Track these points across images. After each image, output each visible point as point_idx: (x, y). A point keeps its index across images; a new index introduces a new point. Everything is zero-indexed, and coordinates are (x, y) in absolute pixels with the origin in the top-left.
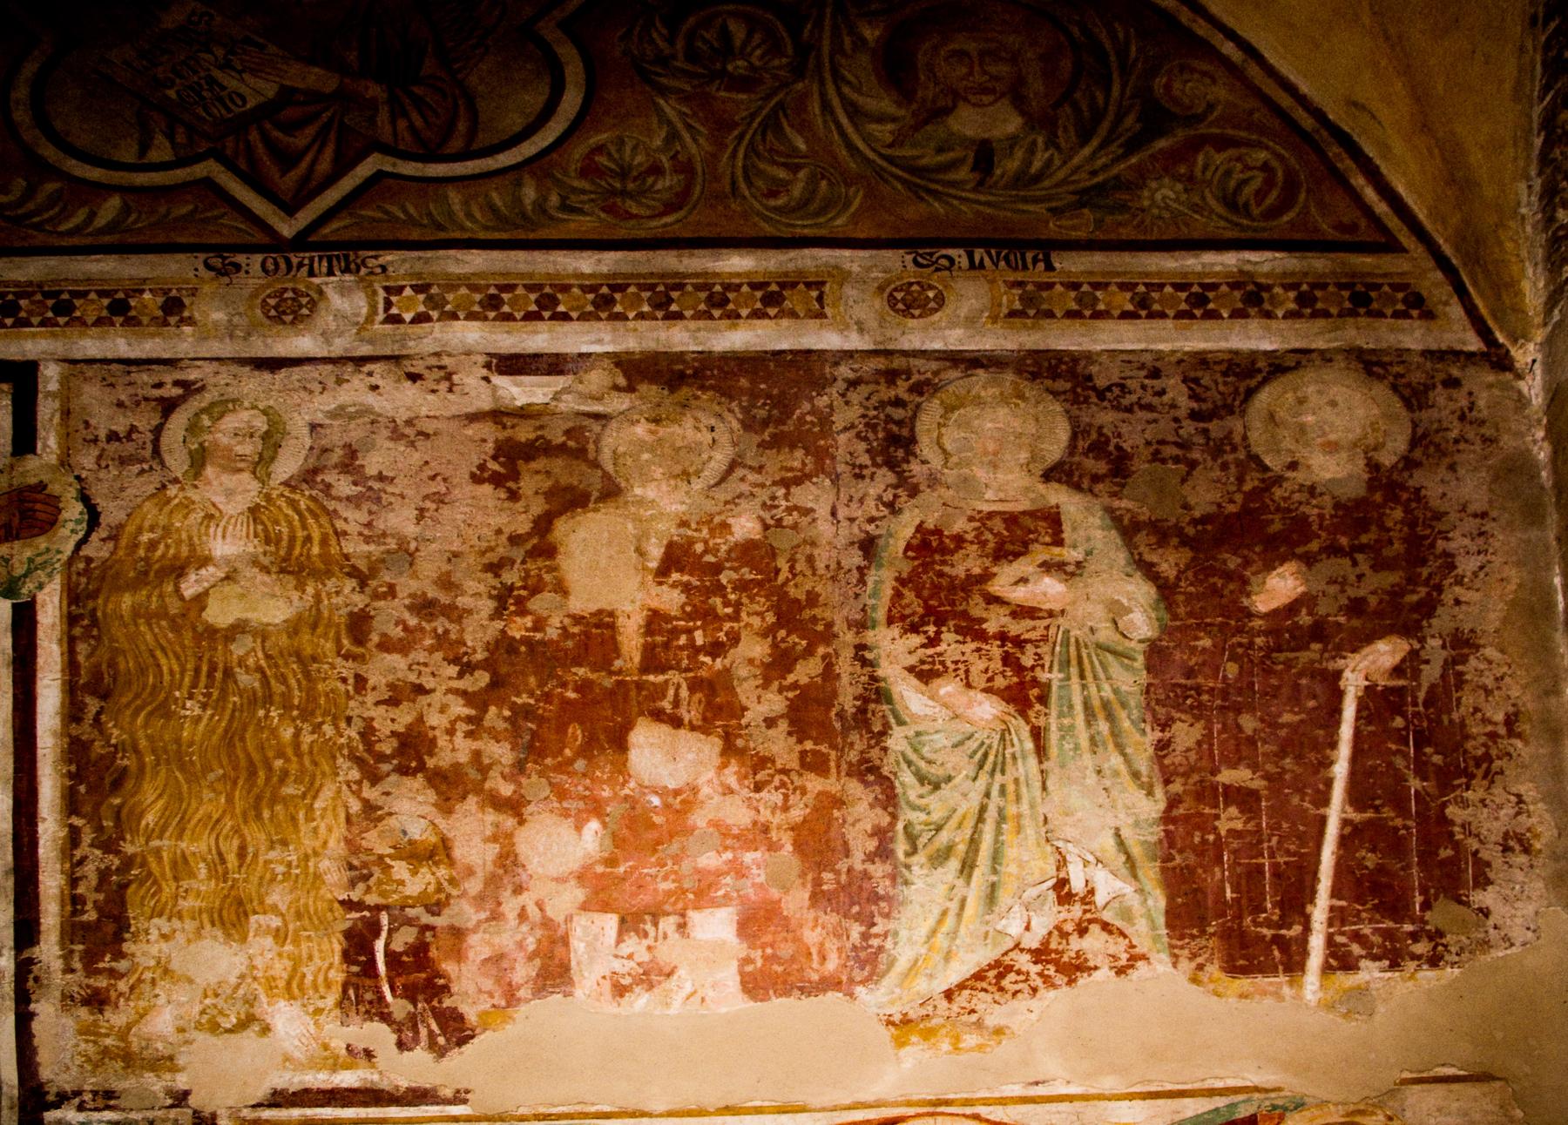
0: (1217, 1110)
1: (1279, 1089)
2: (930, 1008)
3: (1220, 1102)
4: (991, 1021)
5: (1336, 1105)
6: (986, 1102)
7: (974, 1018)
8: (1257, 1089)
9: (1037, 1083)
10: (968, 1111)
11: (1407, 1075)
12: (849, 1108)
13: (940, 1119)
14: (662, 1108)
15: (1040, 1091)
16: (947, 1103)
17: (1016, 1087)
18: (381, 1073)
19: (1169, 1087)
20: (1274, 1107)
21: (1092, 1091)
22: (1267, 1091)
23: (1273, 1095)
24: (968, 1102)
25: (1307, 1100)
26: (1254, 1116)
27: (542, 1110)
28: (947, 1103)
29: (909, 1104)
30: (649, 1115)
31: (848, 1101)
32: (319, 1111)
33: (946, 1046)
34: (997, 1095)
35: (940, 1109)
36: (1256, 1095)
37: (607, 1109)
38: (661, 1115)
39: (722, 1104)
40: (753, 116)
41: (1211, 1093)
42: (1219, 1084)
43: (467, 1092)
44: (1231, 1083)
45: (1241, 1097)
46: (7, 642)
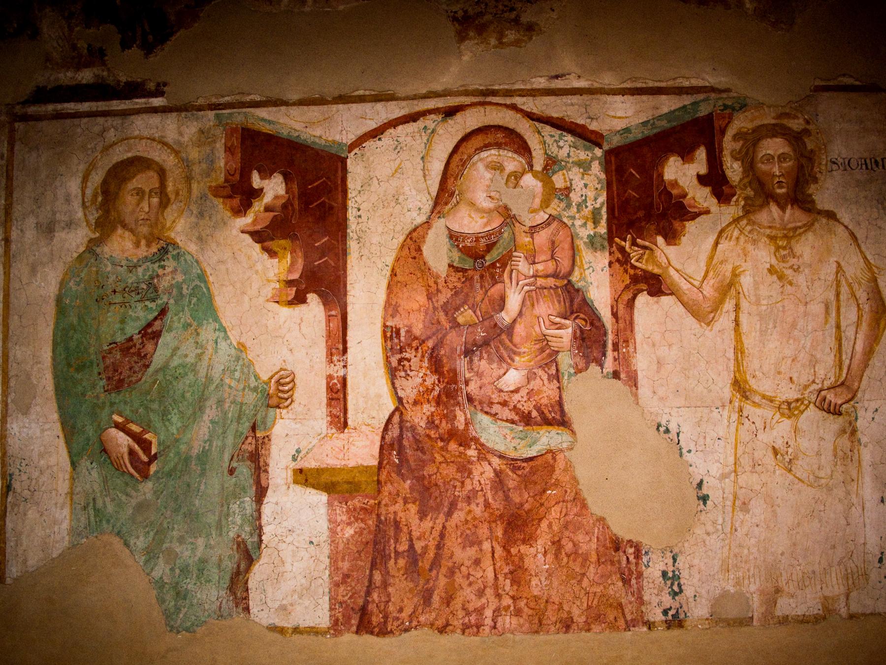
0: (684, 107)
1: (728, 90)
2: (483, 6)
3: (687, 100)
4: (525, 19)
5: (769, 107)
6: (523, 93)
7: (513, 15)
8: (712, 89)
9: (557, 77)
10: (508, 101)
11: (818, 83)
12: (426, 97)
13: (488, 108)
14: (295, 97)
15: (559, 84)
16: (494, 93)
17: (542, 80)
18: (109, 70)
19: (651, 84)
20: (726, 107)
21: (596, 85)
22: (720, 91)
23: (724, 95)
24: (509, 93)
25: (748, 101)
26: (711, 114)
27: (214, 100)
28: (494, 93)
29: (467, 93)
30: (286, 103)
31: (424, 91)
32: (66, 105)
33: (493, 41)
34: (528, 87)
35: (489, 99)
36: (713, 95)
37: (258, 98)
38: (294, 104)
39: (336, 93)
40: (239, 113)
41: (679, 91)
42: (686, 84)
43: (165, 84)
44: (695, 82)
45: (701, 97)
46: (2, 277)
